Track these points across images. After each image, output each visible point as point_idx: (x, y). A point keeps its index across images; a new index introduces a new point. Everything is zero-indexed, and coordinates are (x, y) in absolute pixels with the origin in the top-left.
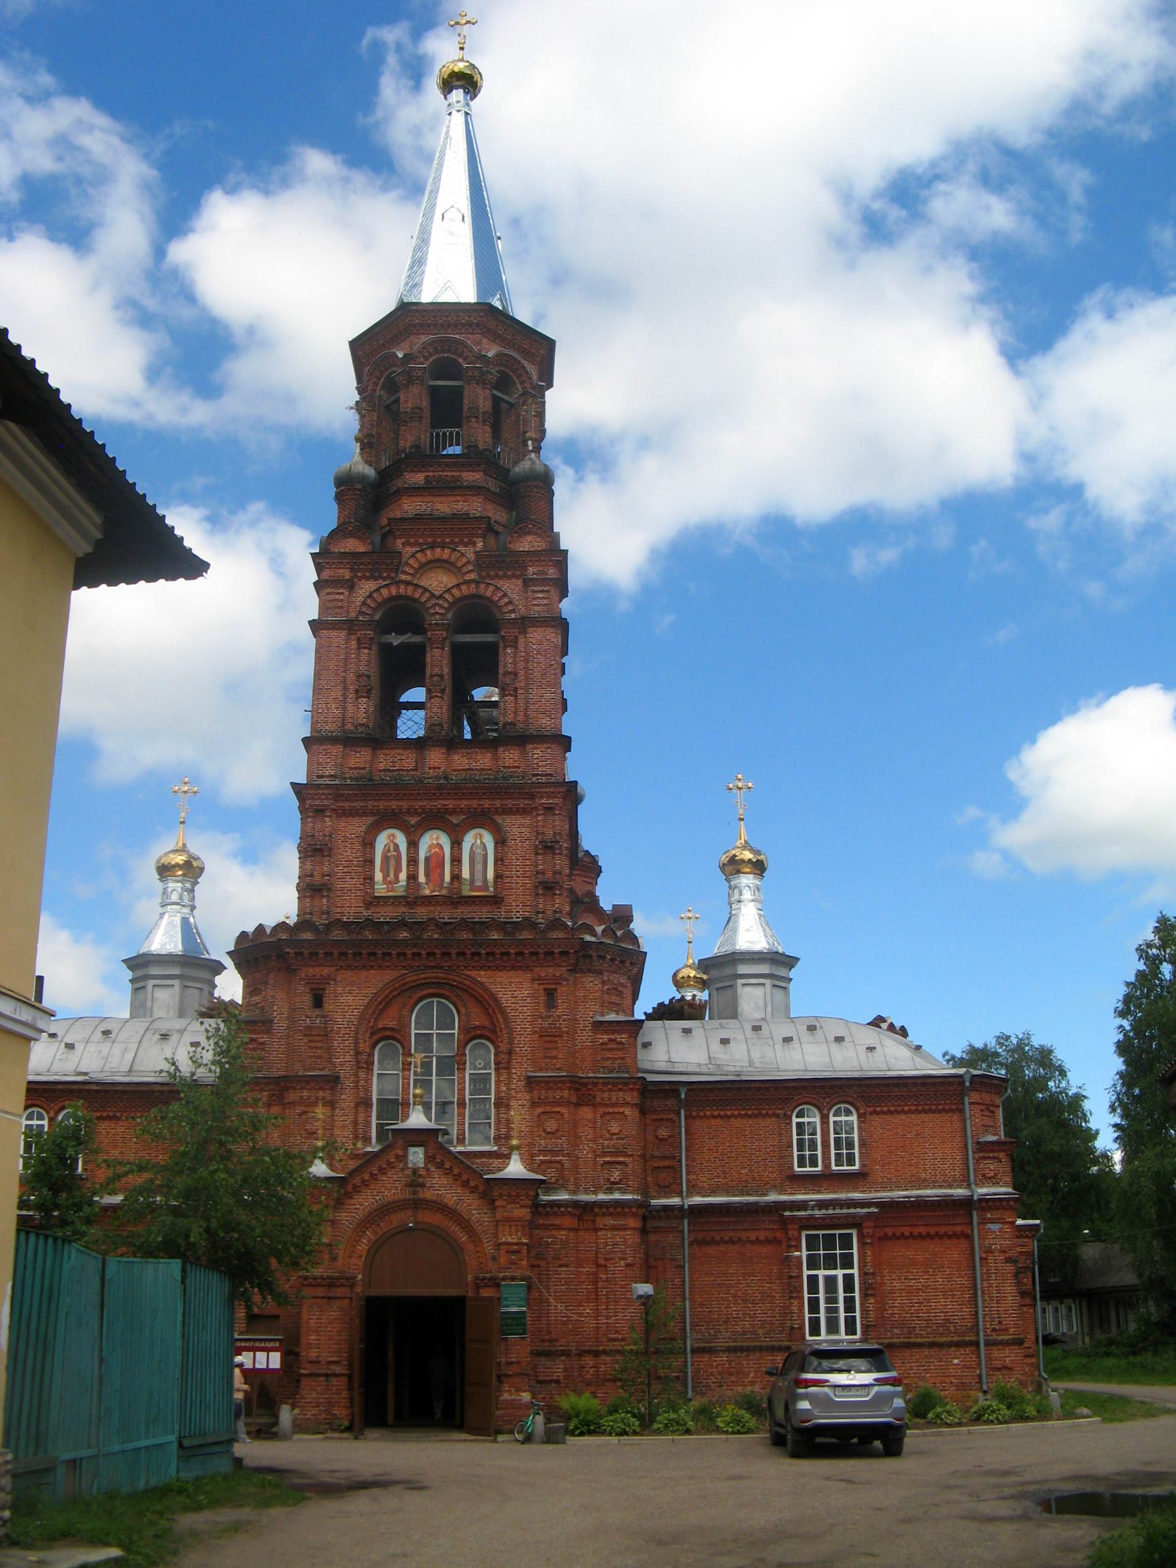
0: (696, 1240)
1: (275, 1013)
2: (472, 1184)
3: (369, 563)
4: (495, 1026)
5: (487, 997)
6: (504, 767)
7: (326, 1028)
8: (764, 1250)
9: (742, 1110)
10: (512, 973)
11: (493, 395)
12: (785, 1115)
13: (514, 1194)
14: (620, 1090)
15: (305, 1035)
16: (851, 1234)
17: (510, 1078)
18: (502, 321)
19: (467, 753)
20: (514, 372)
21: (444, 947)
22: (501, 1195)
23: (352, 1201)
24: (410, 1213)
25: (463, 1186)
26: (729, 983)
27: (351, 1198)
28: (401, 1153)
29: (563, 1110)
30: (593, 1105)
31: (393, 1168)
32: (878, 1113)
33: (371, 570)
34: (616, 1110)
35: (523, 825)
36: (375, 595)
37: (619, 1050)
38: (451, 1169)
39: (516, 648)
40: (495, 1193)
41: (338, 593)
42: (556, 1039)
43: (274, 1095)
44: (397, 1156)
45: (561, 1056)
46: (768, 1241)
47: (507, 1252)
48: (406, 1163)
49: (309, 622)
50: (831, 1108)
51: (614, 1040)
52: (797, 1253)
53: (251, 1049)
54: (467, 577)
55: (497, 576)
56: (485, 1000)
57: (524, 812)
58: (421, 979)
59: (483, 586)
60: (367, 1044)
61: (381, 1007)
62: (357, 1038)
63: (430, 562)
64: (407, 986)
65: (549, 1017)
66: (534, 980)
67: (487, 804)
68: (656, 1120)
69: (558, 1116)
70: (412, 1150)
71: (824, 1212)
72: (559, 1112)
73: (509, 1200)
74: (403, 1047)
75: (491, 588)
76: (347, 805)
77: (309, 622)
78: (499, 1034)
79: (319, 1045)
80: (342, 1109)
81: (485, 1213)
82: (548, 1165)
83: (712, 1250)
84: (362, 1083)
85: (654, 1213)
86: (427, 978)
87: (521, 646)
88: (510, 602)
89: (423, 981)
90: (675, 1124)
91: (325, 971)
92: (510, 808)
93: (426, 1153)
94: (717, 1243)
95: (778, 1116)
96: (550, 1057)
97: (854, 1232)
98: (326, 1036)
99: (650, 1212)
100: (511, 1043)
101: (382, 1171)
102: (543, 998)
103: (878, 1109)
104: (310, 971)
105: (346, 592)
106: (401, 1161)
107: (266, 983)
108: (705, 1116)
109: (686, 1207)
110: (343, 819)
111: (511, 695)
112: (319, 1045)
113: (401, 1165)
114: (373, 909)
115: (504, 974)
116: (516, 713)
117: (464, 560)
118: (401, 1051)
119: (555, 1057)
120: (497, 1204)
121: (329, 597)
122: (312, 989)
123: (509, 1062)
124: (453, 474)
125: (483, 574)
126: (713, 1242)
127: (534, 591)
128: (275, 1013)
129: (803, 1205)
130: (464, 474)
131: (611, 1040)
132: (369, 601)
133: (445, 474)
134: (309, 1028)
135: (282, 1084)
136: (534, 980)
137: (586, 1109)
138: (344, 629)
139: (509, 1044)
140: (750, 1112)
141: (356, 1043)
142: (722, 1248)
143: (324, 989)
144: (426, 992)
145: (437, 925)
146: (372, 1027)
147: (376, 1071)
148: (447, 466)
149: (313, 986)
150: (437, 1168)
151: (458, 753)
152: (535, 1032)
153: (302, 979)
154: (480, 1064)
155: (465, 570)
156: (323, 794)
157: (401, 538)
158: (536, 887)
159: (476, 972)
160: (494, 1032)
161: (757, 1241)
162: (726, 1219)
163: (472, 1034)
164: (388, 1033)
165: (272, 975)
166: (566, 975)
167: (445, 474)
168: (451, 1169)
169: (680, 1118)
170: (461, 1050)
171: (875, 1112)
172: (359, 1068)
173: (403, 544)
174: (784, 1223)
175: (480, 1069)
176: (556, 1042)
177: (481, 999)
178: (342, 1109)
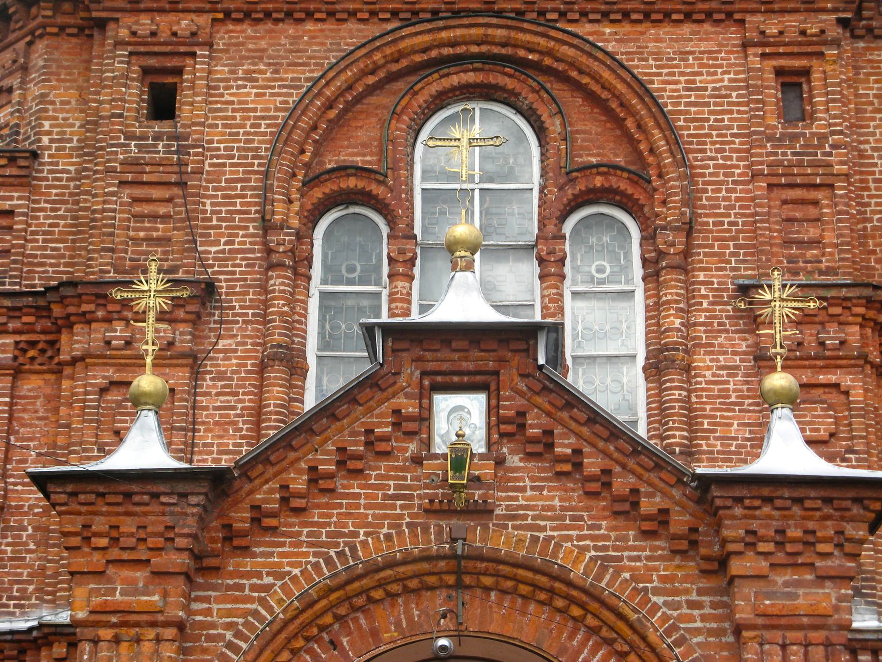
2: (649, 505)
4: (645, 166)
5: (620, 87)
7: (181, 164)
10: (686, 29)
13: (794, 532)
15: (122, 183)
17: (690, 294)
22: (752, 540)
23: (248, 564)
24: (439, 602)
25: (617, 514)
27: (245, 550)
28: (411, 408)
29: (847, 380)
31: (386, 454)
38: (576, 459)
40: (733, 531)
42: (813, 195)
43: (33, 344)
45: (829, 237)
48: (428, 443)
56: (618, 97)
58: (442, 45)
60: (296, 207)
61: (332, 114)
62: (267, 189)
64: (404, 63)
65: (794, 137)
66: (745, 45)
69: (834, 398)
70: (443, 403)
72: (837, 386)
74: (391, 223)
78: (656, 183)
79: (162, 210)
80: (221, 376)
81: (692, 605)
84: (279, 305)
86: (453, 44)
89: (446, 51)
91: (184, 24)
93: (492, 410)
96: (800, 243)
98: (182, 184)
100: (690, 200)
102: (773, 94)
104: (144, 24)
107: (25, 69)
112: (162, 210)
113: (412, 447)
115: (665, 32)
118: (385, 230)
119: (815, 243)
120: (736, 567)
122: (146, 71)
123: (687, 253)
128: (45, 140)
134: (132, 164)
135: (57, 310)
136: (745, 45)
139: (685, 203)
141: (266, 200)
143: (178, 72)
144: (455, 80)
146: (307, 166)
147: (316, 286)
149: (152, 62)
150: (530, 456)
152: (756, 176)
153: (119, 43)
154: (601, 270)
160: (640, 178)
163: (581, 186)
164: (352, 182)
165: (40, 46)
166: (834, 32)
168: (576, 459)
170: (551, 228)
172: (271, 267)
175: (601, 282)
176: (815, 203)
177: (605, 95)
178: (221, 376)
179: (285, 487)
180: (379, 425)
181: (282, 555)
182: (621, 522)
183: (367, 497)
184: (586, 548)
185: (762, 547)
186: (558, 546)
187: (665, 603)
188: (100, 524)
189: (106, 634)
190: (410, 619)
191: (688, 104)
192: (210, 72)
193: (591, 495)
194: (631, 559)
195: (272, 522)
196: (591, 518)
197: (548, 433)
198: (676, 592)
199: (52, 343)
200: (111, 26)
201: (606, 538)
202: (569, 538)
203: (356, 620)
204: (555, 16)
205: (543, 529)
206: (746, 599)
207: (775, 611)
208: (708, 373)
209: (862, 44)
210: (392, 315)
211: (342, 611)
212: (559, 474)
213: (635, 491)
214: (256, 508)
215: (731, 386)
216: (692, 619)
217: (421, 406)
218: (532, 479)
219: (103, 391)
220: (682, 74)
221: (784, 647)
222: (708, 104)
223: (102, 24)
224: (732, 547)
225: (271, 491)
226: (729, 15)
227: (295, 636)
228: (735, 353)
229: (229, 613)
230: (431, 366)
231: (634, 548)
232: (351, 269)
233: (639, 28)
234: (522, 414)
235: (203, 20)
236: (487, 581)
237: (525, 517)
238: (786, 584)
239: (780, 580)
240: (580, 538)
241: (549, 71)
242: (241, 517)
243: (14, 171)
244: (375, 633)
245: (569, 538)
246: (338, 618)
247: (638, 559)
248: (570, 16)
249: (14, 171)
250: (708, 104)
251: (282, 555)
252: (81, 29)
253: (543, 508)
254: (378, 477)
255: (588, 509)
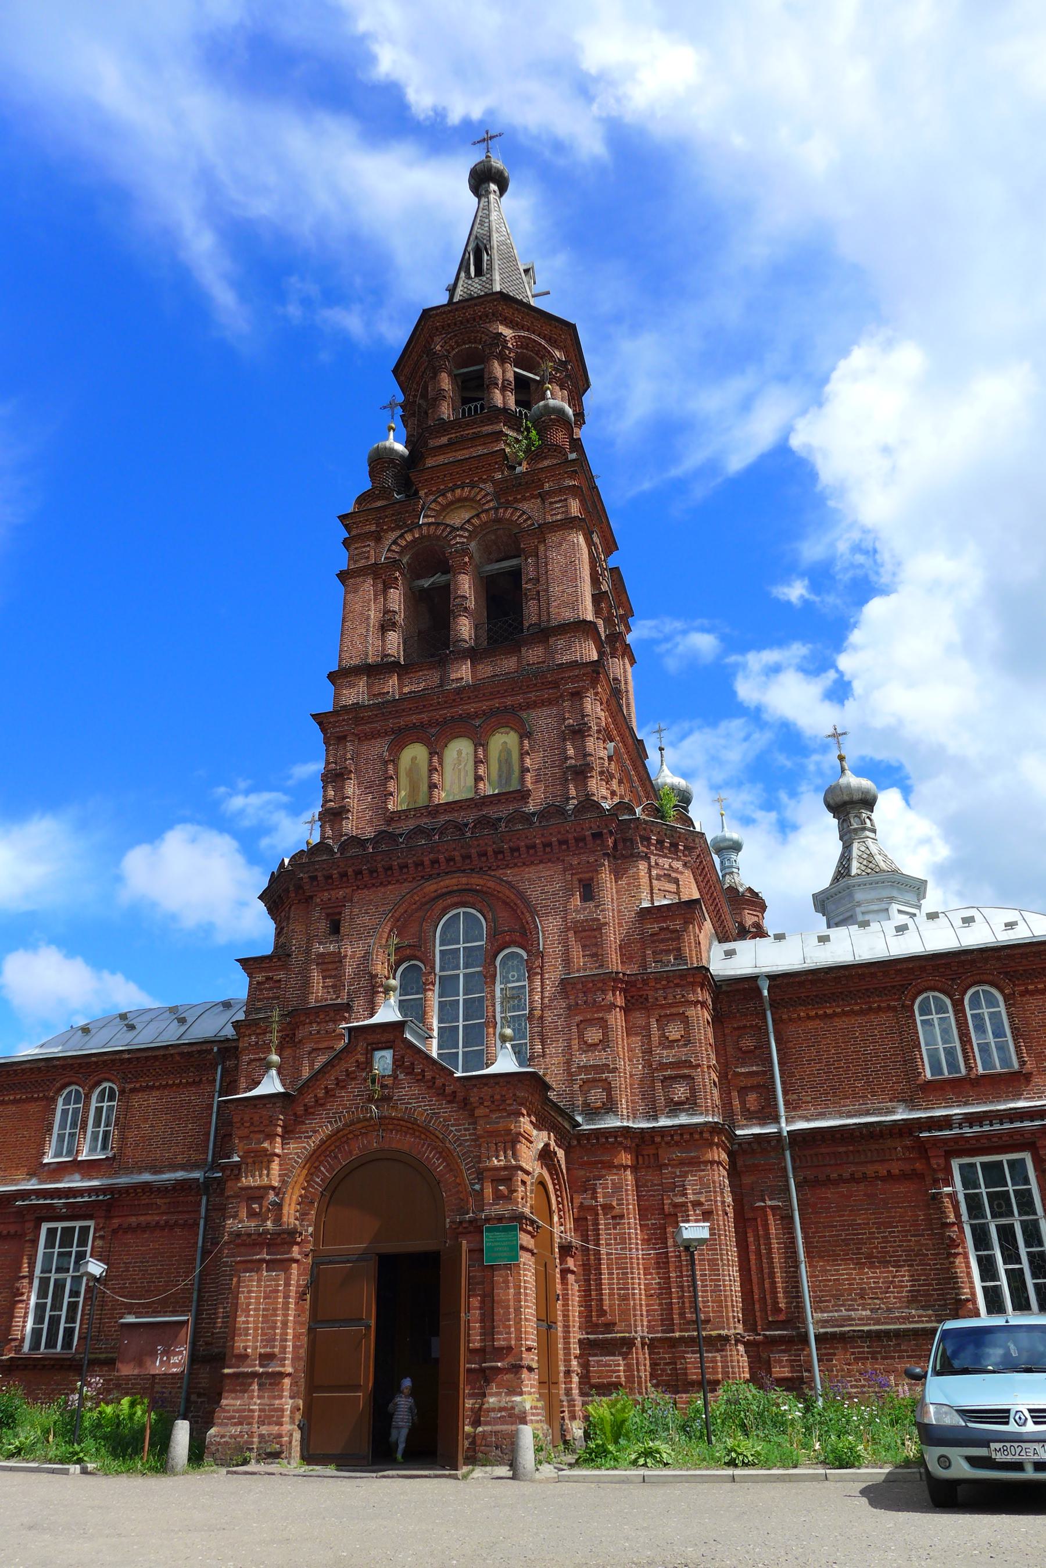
0: (806, 1180)
1: (294, 948)
3: (393, 515)
6: (528, 665)
8: (900, 1189)
9: (846, 1006)
10: (541, 866)
11: (515, 372)
12: (903, 1006)
14: (677, 985)
16: (1023, 1160)
18: (517, 309)
19: (491, 661)
20: (537, 354)
21: (462, 847)
23: (304, 1128)
25: (438, 1095)
26: (848, 914)
27: (303, 1123)
28: (362, 1059)
30: (646, 1009)
32: (1032, 993)
33: (395, 520)
34: (674, 1010)
35: (550, 716)
36: (399, 541)
37: (673, 940)
39: (537, 556)
41: (364, 547)
43: (287, 1035)
44: (358, 1064)
46: (905, 1176)
47: (492, 1181)
49: (337, 575)
50: (964, 993)
51: (667, 928)
52: (948, 1189)
53: (266, 989)
54: (486, 507)
55: (516, 501)
57: (549, 702)
59: (501, 510)
63: (452, 503)
65: (585, 909)
66: (565, 870)
67: (509, 701)
68: (739, 1028)
70: (378, 1054)
71: (977, 1129)
73: (493, 1107)
75: (510, 511)
76: (367, 728)
77: (337, 575)
81: (466, 1130)
82: (590, 1085)
83: (829, 1193)
85: (745, 1146)
87: (541, 554)
88: (530, 518)
90: (401, 693)
92: (535, 702)
94: (836, 1183)
95: (894, 1009)
97: (1027, 1156)
99: (740, 1144)
101: (340, 1084)
103: (1030, 987)
105: (372, 544)
106: (363, 1070)
107: (288, 918)
108: (800, 1018)
109: (785, 1134)
110: (365, 743)
111: (534, 599)
114: (394, 825)
115: (533, 869)
116: (539, 615)
117: (483, 493)
120: (478, 1112)
121: (356, 552)
122: (328, 915)
124: (474, 430)
125: (503, 500)
126: (828, 1182)
127: (551, 503)
129: (946, 1122)
130: (484, 429)
131: (662, 929)
132: (394, 547)
133: (467, 432)
137: (638, 1014)
138: (369, 574)
140: (856, 1008)
142: (843, 1189)
143: (340, 913)
145: (456, 827)
148: (467, 425)
149: (330, 911)
150: (407, 1074)
151: (482, 663)
153: (318, 905)
155: (484, 501)
156: (344, 720)
157: (423, 490)
158: (565, 773)
159: (501, 871)
161: (890, 1177)
162: (842, 1149)
167: (467, 432)
169: (766, 1022)
171: (1026, 992)
173: (426, 493)
174: (923, 1148)
175: (513, 982)
179: (316, 1096)
180: (350, 1067)
181: (315, 1123)
182: (440, 1097)
183: (347, 1096)
184: (427, 1110)
185: (486, 1104)
186: (415, 1110)
187: (456, 1130)
188: (247, 1118)
189: (250, 1160)
190: (363, 1144)
191: (541, 900)
192: (351, 912)
193: (429, 1087)
194: (443, 1112)
195: (312, 1110)
196: (429, 1097)
197: (413, 1064)
198: (460, 1125)
199: (294, 1034)
200: (315, 898)
201: (435, 1105)
202: (420, 1106)
203: (344, 1147)
204: (486, 869)
205: (411, 1103)
206: (481, 1126)
207: (491, 1130)
208: (549, 1019)
209: (620, 861)
210: (525, 980)
211: (337, 1144)
212: (418, 1080)
213: (444, 1085)
214: (305, 1105)
215: (559, 1023)
216: (465, 1135)
217: (367, 1058)
218: (408, 1083)
219: (310, 1053)
220: (539, 887)
221: (496, 1144)
222: (550, 899)
223: (311, 897)
224: (475, 1105)
225: (311, 1098)
226: (558, 859)
227: (320, 1155)
228: (561, 1008)
229: (296, 1148)
230: (370, 1041)
231: (445, 1108)
232: (412, 989)
233: (522, 869)
234: (403, 1057)
235: (348, 890)
236: (390, 1127)
237: (404, 1099)
238: (496, 1118)
239: (494, 1116)
240: (425, 1106)
241: (486, 893)
242: (300, 1110)
243: (281, 963)
244: (350, 1152)
245: (420, 1106)
246: (336, 1147)
247: (446, 1112)
248: (493, 868)
249: (281, 963)
250: (550, 899)
251: (315, 1123)
252: (306, 900)
253: (412, 1095)
254: (352, 1088)
255: (428, 1094)
